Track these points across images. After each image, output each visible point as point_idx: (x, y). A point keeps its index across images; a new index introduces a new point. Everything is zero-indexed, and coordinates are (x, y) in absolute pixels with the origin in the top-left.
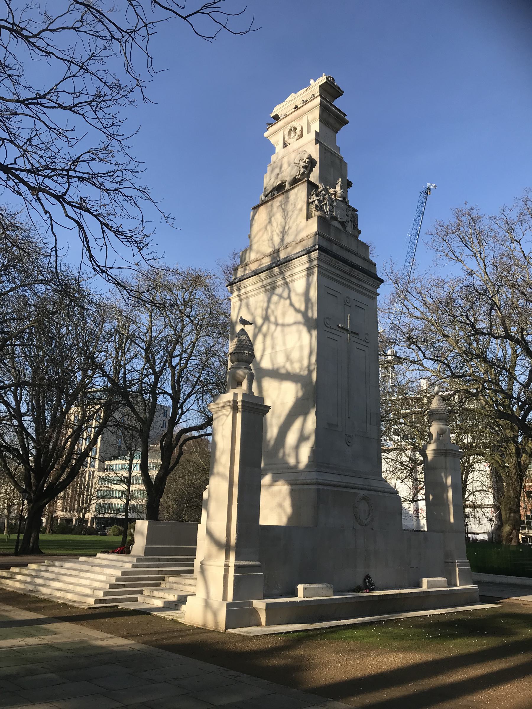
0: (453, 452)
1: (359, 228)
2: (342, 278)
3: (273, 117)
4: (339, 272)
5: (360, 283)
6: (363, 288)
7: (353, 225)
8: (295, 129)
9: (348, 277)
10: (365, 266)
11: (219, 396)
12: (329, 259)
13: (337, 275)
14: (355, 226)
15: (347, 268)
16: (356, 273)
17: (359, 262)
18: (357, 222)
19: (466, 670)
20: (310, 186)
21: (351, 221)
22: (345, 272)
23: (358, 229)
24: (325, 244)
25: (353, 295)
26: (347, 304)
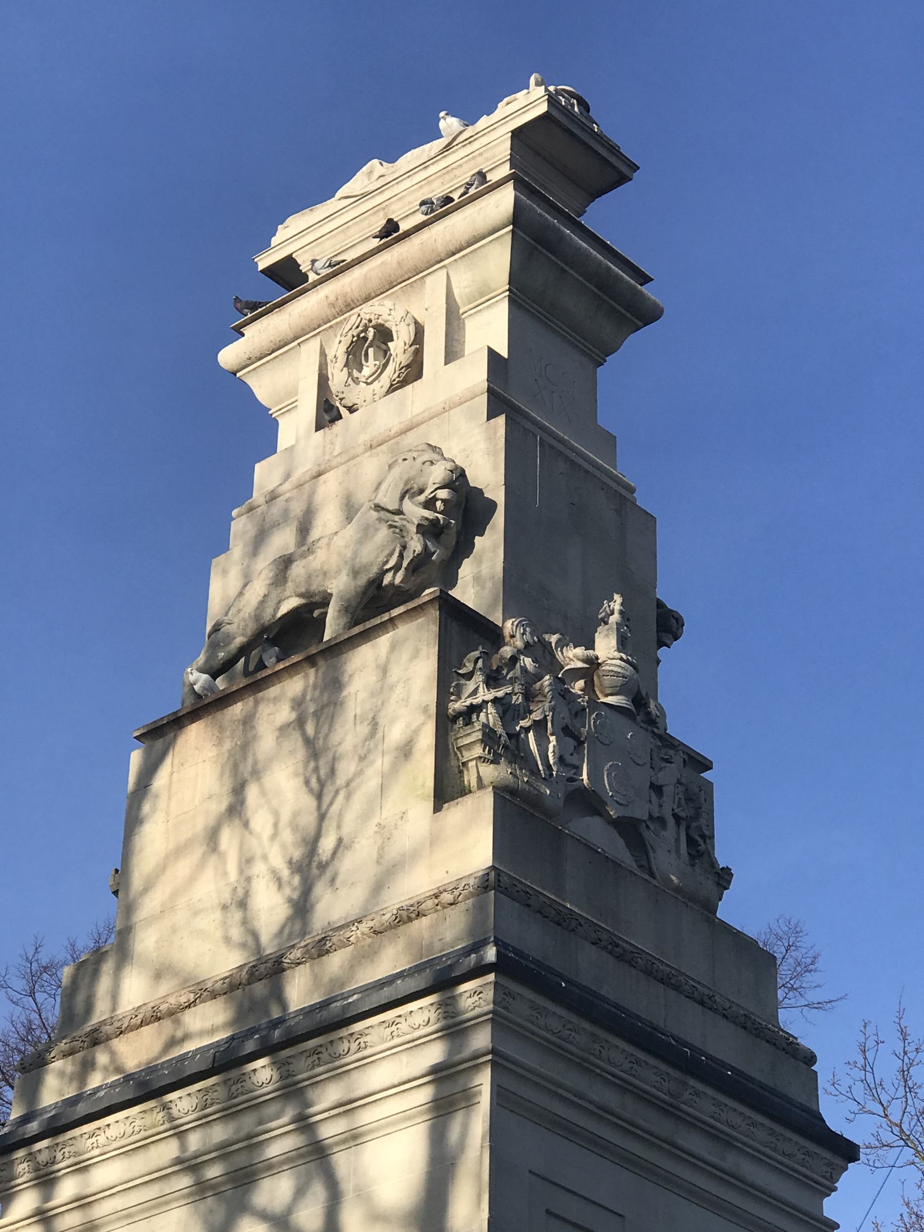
2: (629, 1129)
4: (611, 1099)
5: (731, 1161)
7: (691, 842)
8: (384, 335)
9: (663, 1126)
10: (756, 1064)
13: (601, 1112)
14: (699, 844)
15: (653, 1075)
16: (706, 1102)
17: (724, 1045)
20: (455, 627)
22: (643, 1097)
23: (713, 863)
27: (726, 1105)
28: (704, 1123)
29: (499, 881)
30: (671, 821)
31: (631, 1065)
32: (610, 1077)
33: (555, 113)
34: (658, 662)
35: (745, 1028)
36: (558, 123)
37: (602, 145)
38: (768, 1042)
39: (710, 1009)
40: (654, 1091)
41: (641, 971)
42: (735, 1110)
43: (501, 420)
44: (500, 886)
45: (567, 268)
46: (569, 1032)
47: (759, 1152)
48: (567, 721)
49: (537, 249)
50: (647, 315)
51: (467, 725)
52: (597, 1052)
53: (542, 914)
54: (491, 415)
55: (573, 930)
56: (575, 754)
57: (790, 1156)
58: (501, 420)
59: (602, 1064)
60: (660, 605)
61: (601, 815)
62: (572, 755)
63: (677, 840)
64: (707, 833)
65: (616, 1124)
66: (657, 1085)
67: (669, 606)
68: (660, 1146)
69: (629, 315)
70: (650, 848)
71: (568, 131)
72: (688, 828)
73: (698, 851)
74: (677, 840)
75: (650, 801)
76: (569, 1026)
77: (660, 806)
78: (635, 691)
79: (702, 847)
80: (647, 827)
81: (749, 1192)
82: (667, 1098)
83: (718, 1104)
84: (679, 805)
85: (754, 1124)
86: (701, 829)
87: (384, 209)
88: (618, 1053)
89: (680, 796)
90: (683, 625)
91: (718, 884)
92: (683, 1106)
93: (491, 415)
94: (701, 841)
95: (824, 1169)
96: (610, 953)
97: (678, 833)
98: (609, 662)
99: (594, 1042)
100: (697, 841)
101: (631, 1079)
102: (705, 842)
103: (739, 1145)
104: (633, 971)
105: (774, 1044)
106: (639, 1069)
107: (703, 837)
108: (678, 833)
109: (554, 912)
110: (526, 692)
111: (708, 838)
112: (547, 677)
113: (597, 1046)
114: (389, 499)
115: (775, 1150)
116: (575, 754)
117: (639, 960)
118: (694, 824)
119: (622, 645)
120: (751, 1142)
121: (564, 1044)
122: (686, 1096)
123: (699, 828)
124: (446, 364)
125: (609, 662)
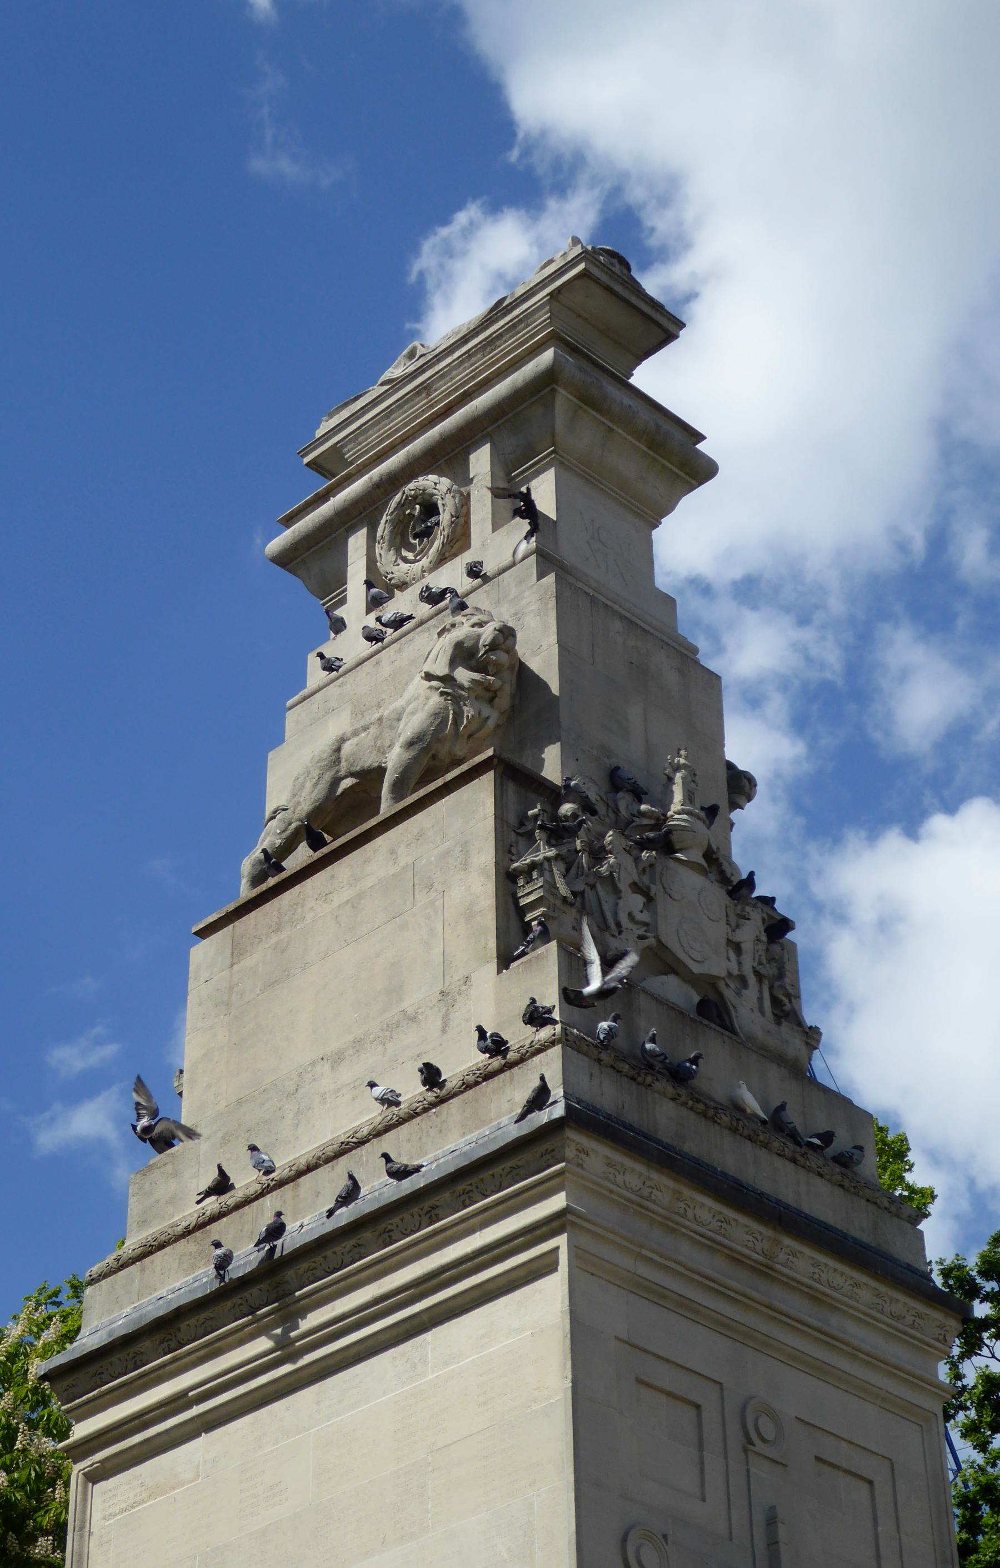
0: (670, 1224)
1: (810, 1018)
2: (721, 1292)
3: (308, 465)
6: (855, 1353)
7: (775, 1002)
8: (431, 509)
10: (856, 1222)
11: (737, 573)
12: (634, 1182)
14: (785, 1008)
15: (745, 1232)
16: (804, 1261)
17: (818, 1198)
18: (796, 985)
19: (310, 526)
20: (511, 788)
21: (759, 976)
22: (737, 1260)
23: (799, 1022)
24: (608, 1094)
25: (795, 1394)
26: (760, 1446)
27: (826, 1265)
28: (802, 1284)
29: (566, 1035)
30: (752, 980)
31: (720, 1224)
32: (697, 1237)
33: (596, 271)
34: (732, 825)
35: (842, 1186)
36: (597, 281)
37: (646, 302)
38: (868, 1200)
39: (803, 1167)
40: (746, 1251)
41: (725, 1128)
42: (835, 1270)
43: (550, 579)
44: (567, 1040)
45: (615, 428)
46: (650, 1190)
47: (865, 1314)
48: (635, 877)
49: (580, 407)
50: (699, 471)
51: (528, 883)
52: (682, 1211)
53: (614, 1068)
54: (541, 576)
55: (650, 1085)
56: (645, 911)
57: (899, 1318)
58: (550, 579)
59: (688, 1223)
60: (730, 766)
61: (676, 973)
62: (642, 912)
63: (760, 999)
64: (791, 991)
65: (706, 1285)
66: (750, 1244)
67: (740, 768)
68: (757, 1309)
69: (682, 474)
70: (731, 1008)
71: (609, 289)
72: (771, 988)
73: (783, 1011)
74: (760, 999)
75: (728, 959)
76: (649, 1183)
77: (740, 963)
78: (706, 846)
79: (788, 1007)
80: (727, 985)
81: (592, 483)
82: (760, 1258)
83: (816, 1265)
84: (760, 963)
85: (857, 1285)
86: (785, 989)
87: (425, 388)
88: (705, 1209)
89: (760, 953)
90: (755, 785)
91: (807, 1043)
92: (778, 1267)
93: (541, 576)
94: (786, 1001)
95: (939, 1331)
96: (691, 1109)
97: (761, 992)
98: (677, 816)
99: (678, 1199)
100: (782, 1001)
101: (720, 1238)
102: (790, 1001)
103: (845, 1308)
104: (717, 1127)
105: (876, 1203)
106: (728, 1227)
107: (788, 995)
108: (761, 992)
109: (627, 1067)
110: (590, 848)
111: (794, 996)
112: (611, 833)
113: (682, 1205)
114: (441, 669)
115: (882, 1312)
116: (645, 911)
117: (723, 1116)
118: (778, 983)
119: (690, 800)
120: (855, 1304)
121: (646, 1203)
122: (782, 1257)
123: (783, 987)
124: (493, 531)
125: (677, 816)
